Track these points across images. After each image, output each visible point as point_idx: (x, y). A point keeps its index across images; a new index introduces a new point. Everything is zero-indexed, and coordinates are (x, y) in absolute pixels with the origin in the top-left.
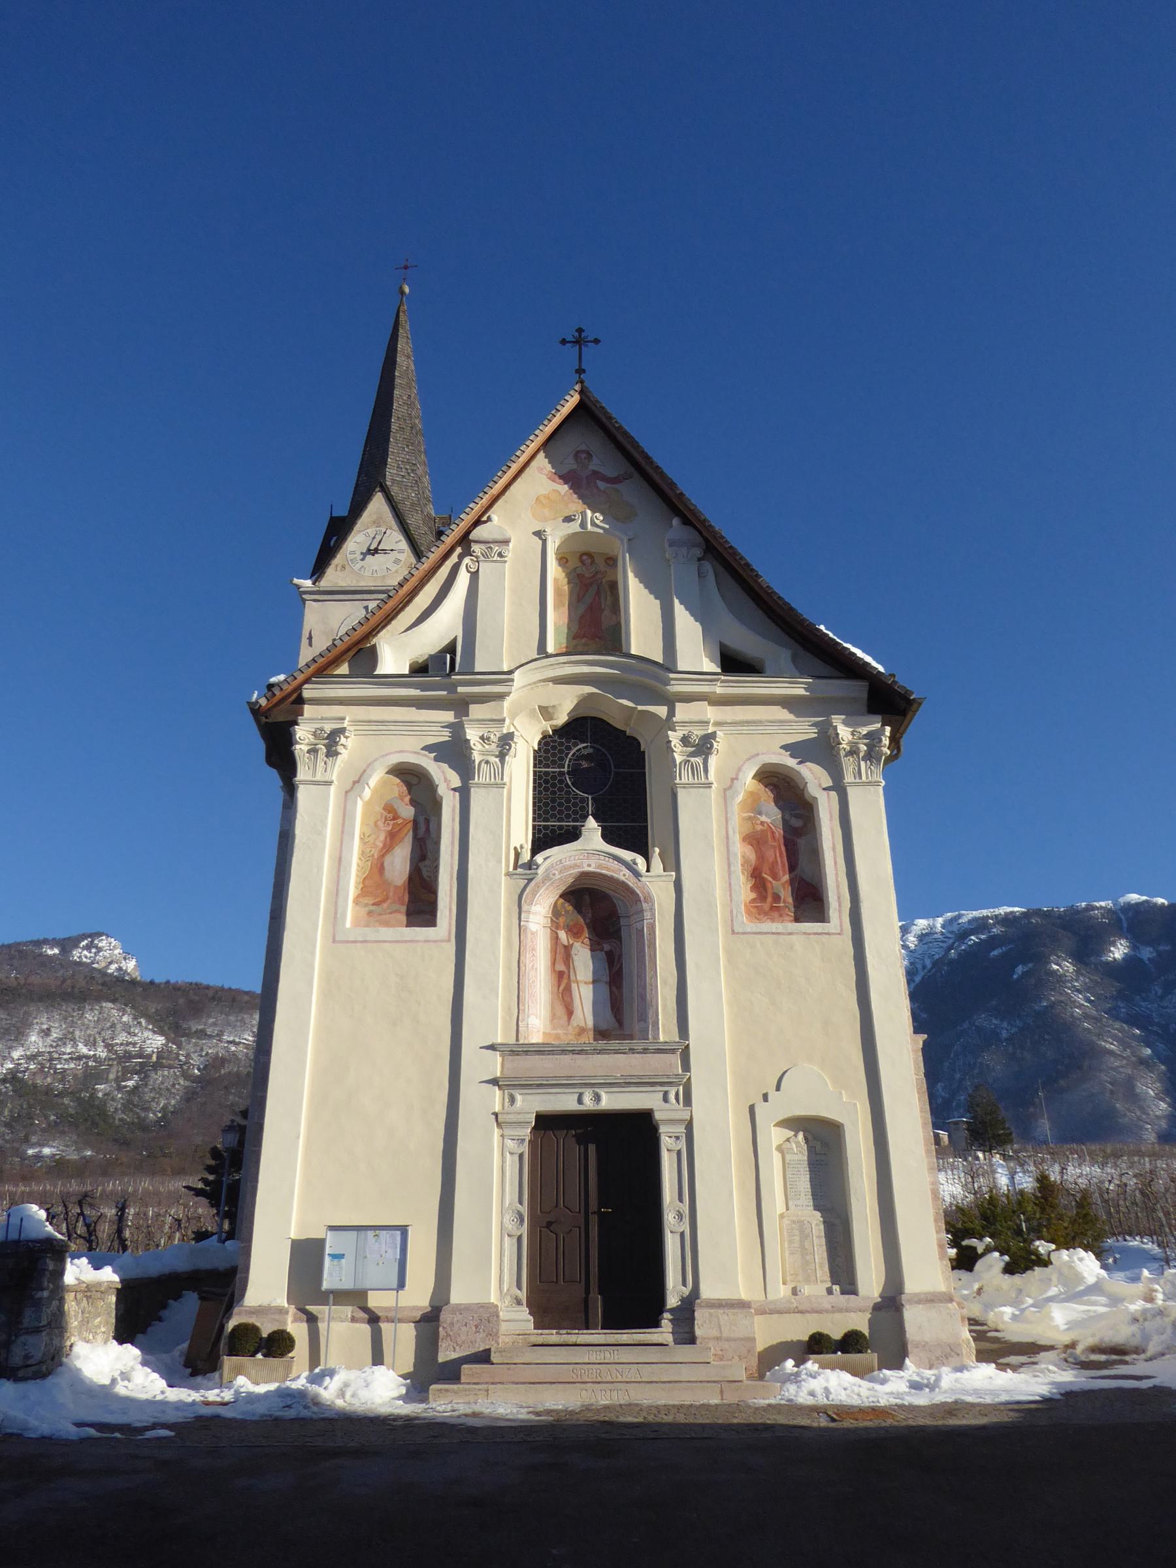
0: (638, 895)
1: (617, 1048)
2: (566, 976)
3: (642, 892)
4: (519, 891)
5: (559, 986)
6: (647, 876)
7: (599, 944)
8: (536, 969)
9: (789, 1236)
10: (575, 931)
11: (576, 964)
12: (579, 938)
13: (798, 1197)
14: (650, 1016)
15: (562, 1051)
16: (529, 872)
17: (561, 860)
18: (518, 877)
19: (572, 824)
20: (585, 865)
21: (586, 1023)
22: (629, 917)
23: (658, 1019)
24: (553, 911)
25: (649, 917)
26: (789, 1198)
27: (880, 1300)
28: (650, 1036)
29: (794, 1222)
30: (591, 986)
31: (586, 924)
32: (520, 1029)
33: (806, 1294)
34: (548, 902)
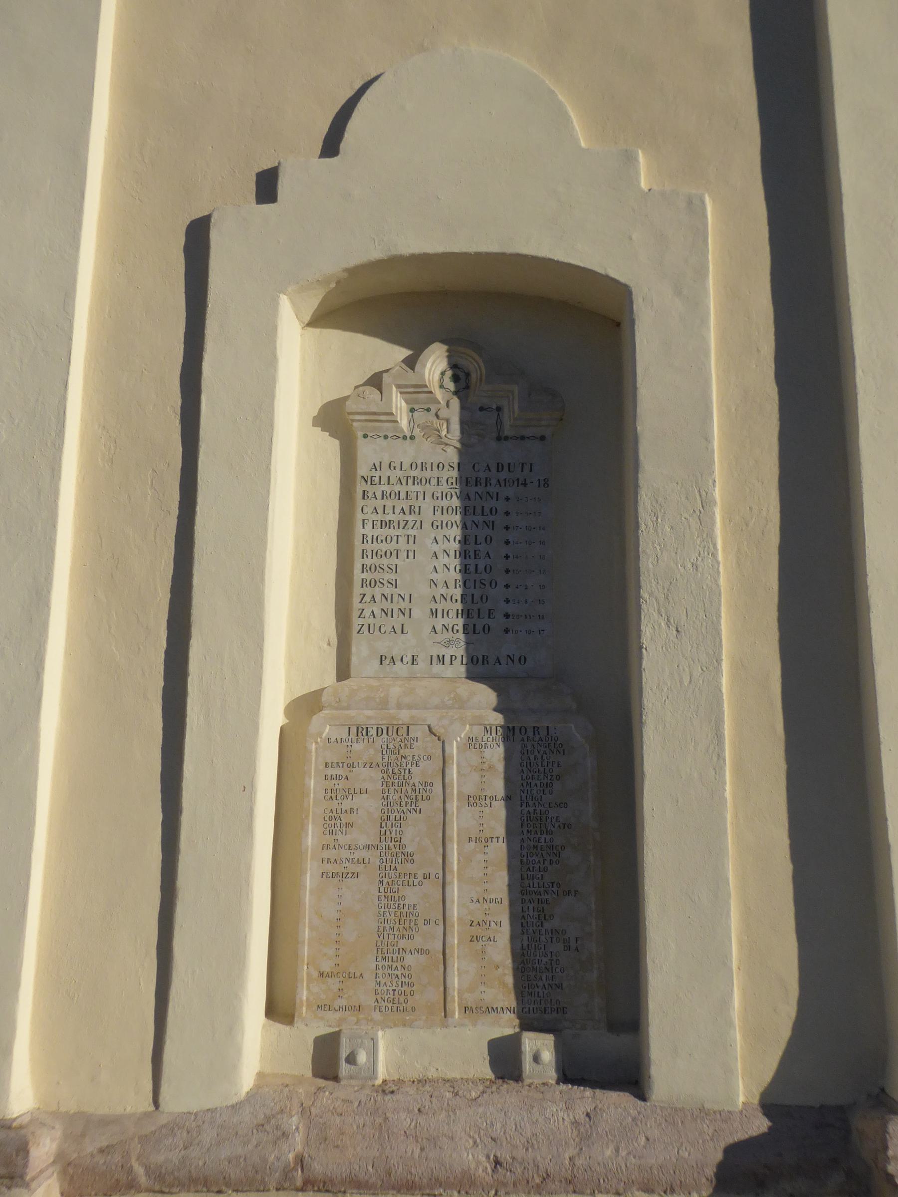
9: (331, 795)
13: (397, 620)
26: (356, 622)
27: (760, 1125)
29: (362, 731)
33: (382, 1073)
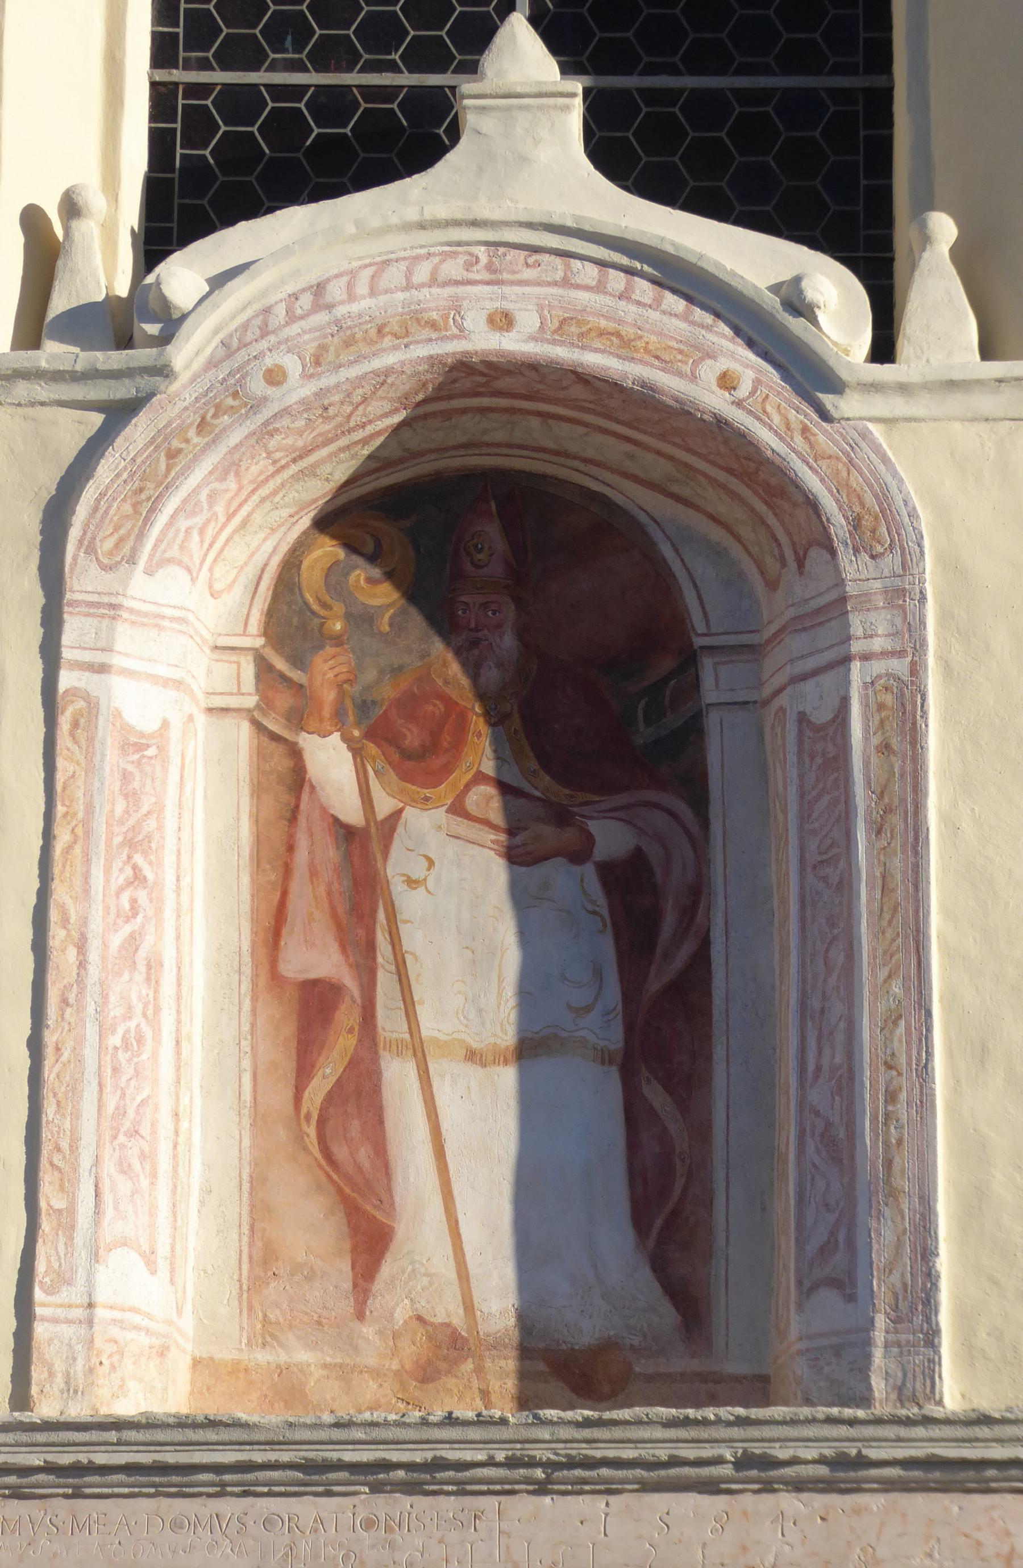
0: (813, 505)
1: (663, 1453)
2: (347, 1016)
3: (841, 488)
4: (48, 481)
5: (304, 1072)
6: (874, 387)
7: (562, 817)
8: (153, 968)
10: (413, 737)
11: (413, 939)
12: (434, 778)
14: (880, 1256)
15: (309, 1467)
16: (115, 359)
17: (319, 289)
18: (42, 391)
19: (406, 79)
20: (475, 321)
21: (469, 1307)
22: (754, 651)
23: (931, 1277)
24: (270, 614)
25: (878, 644)
28: (878, 1385)
30: (508, 1077)
31: (481, 696)
32: (40, 1330)
34: (238, 553)
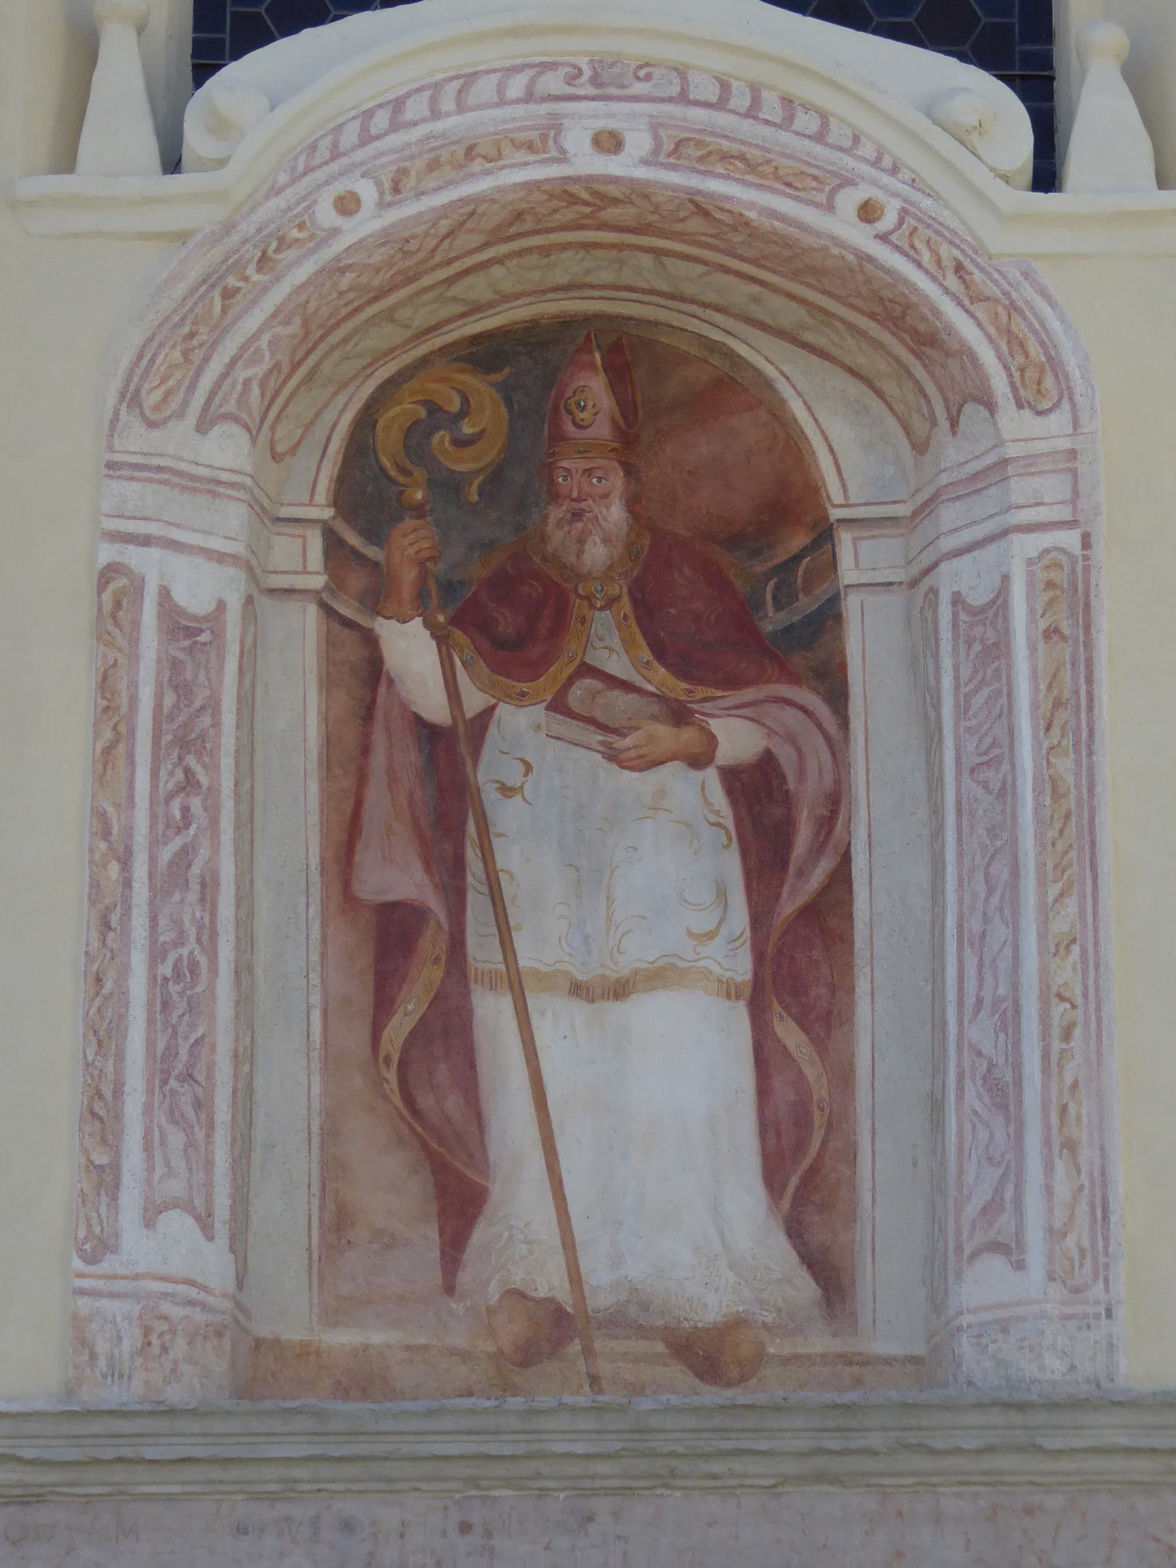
7: (679, 715)
8: (209, 886)
12: (533, 669)
17: (398, 105)
